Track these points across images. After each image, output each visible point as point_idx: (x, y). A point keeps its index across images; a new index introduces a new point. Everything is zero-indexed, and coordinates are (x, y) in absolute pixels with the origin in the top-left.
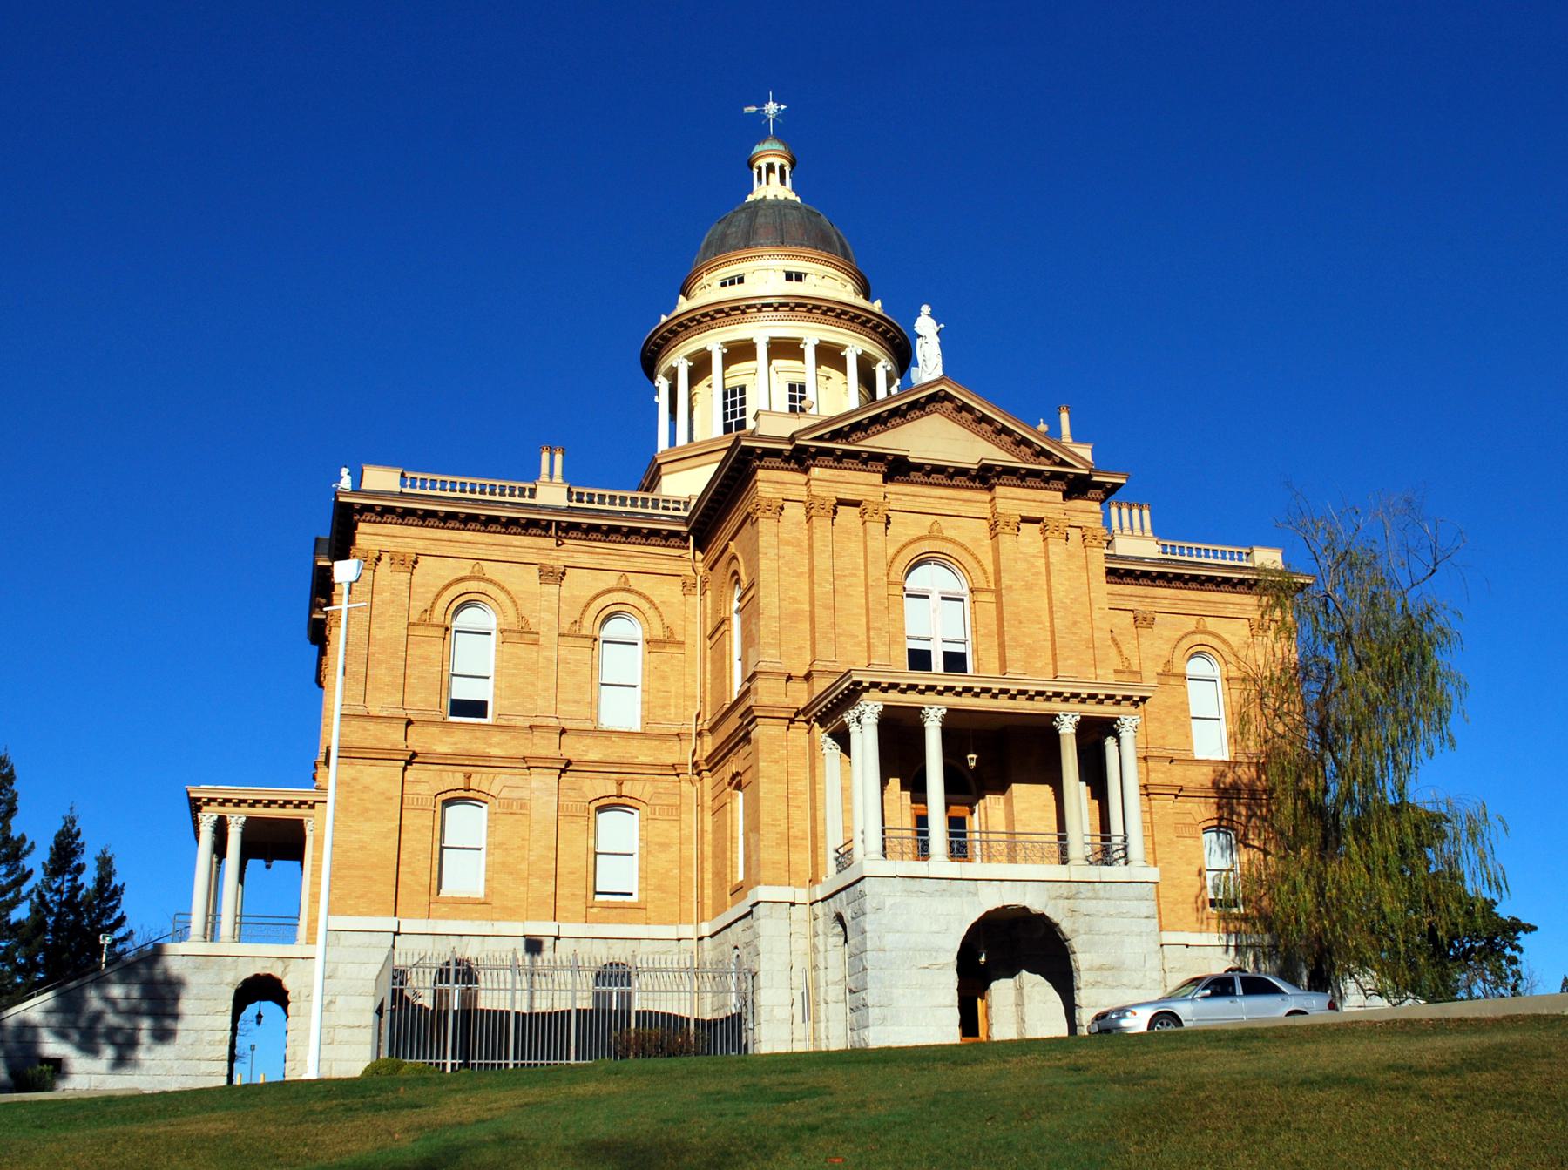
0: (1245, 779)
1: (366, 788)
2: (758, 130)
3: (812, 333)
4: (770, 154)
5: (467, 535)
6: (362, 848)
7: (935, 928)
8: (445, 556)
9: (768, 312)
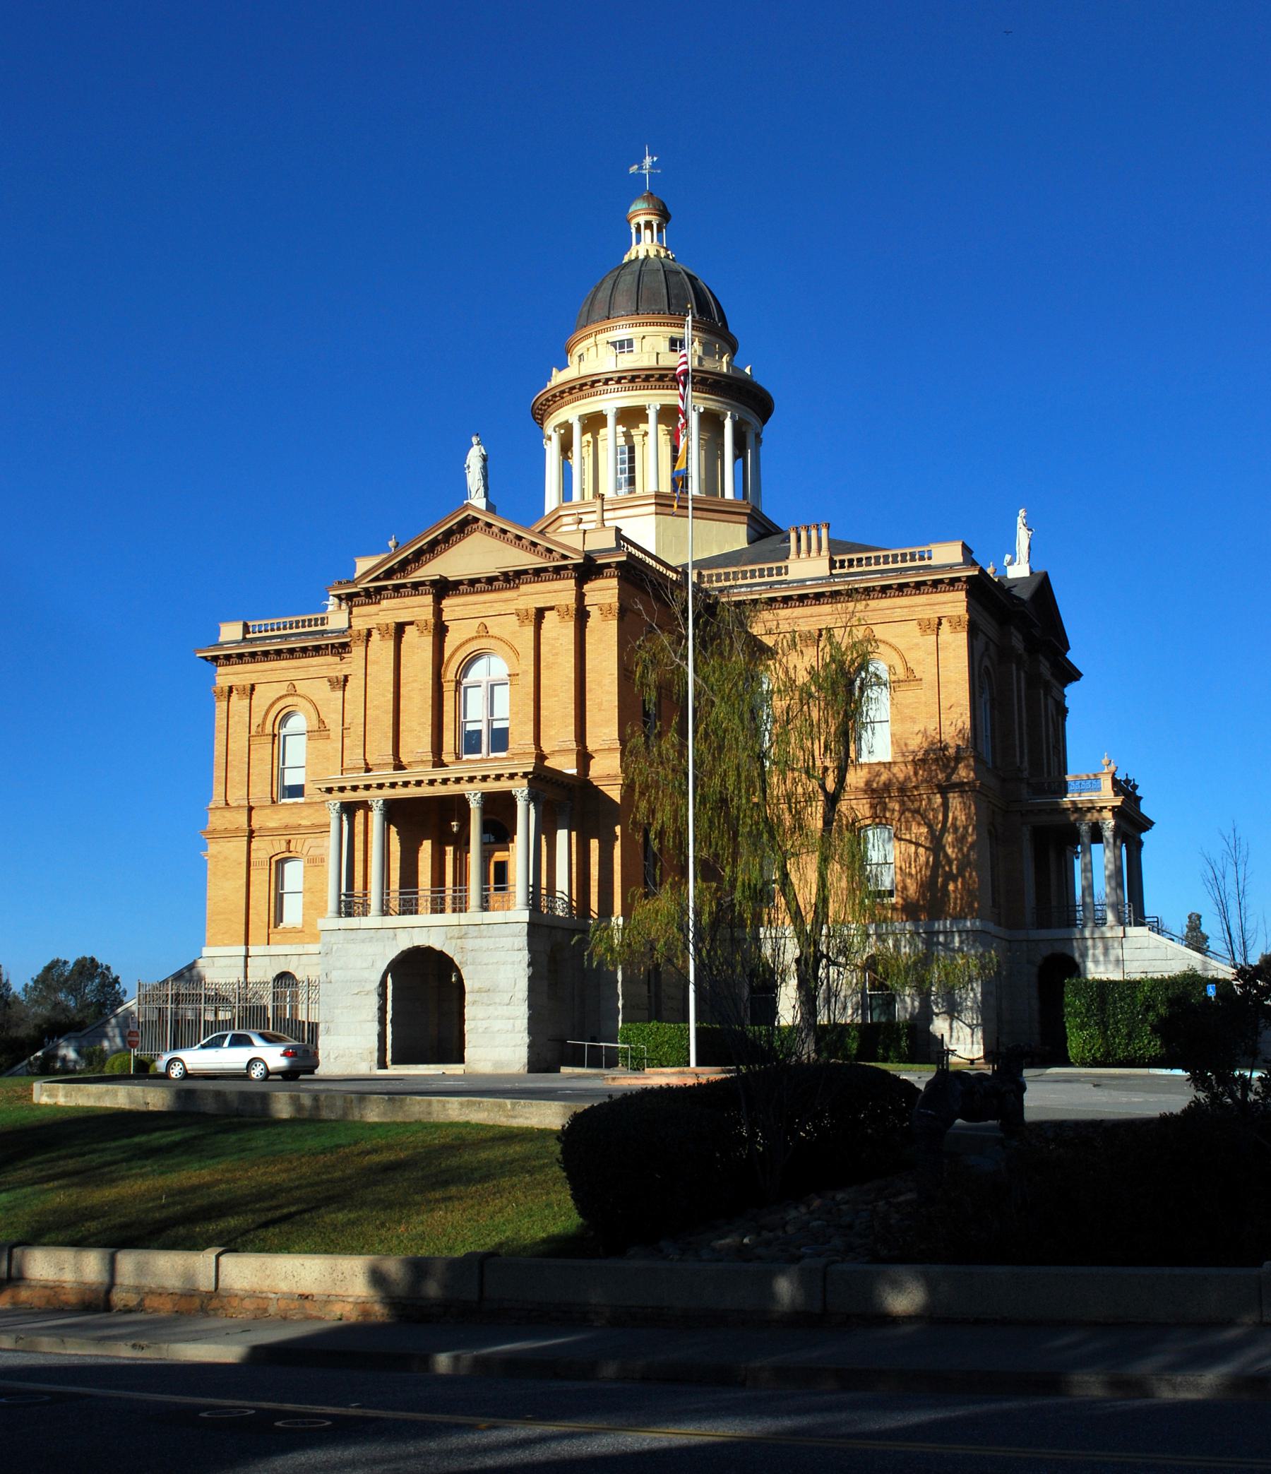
0: (901, 776)
1: (226, 858)
2: (634, 188)
3: (653, 400)
4: (640, 214)
5: (283, 663)
6: (225, 900)
7: (365, 965)
8: (270, 679)
9: (612, 386)
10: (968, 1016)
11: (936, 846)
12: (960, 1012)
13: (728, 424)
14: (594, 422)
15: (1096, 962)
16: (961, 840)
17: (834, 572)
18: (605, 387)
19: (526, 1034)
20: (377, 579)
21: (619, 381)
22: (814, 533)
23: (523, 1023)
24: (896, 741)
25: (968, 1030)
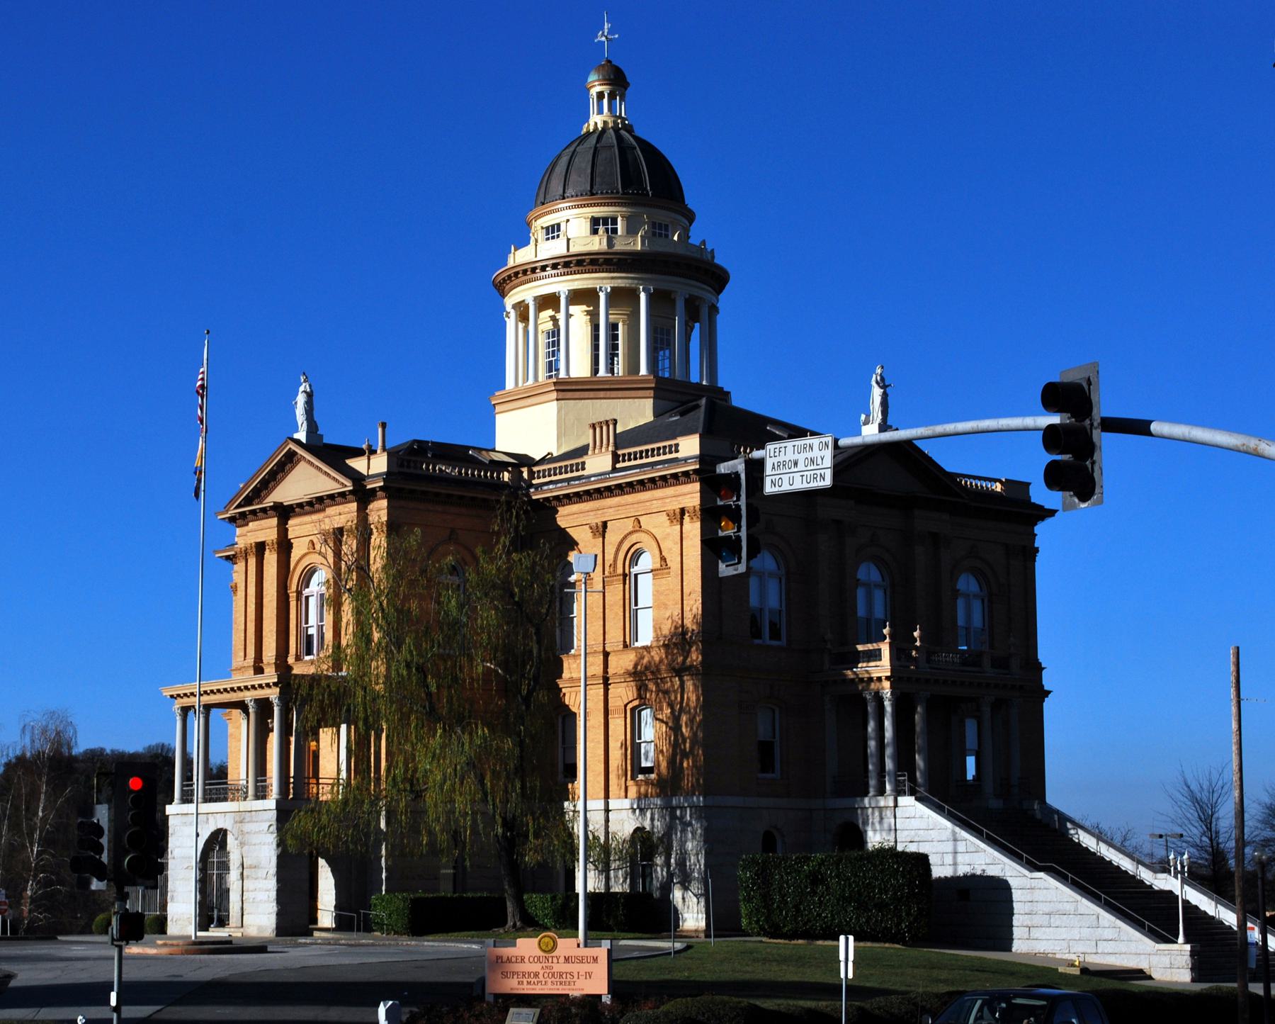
10: (695, 887)
11: (675, 728)
12: (690, 882)
13: (643, 296)
14: (549, 301)
15: (875, 831)
16: (692, 720)
17: (618, 466)
18: (544, 274)
19: (275, 904)
20: (239, 506)
21: (555, 266)
22: (605, 428)
23: (273, 894)
24: (657, 628)
25: (695, 900)
